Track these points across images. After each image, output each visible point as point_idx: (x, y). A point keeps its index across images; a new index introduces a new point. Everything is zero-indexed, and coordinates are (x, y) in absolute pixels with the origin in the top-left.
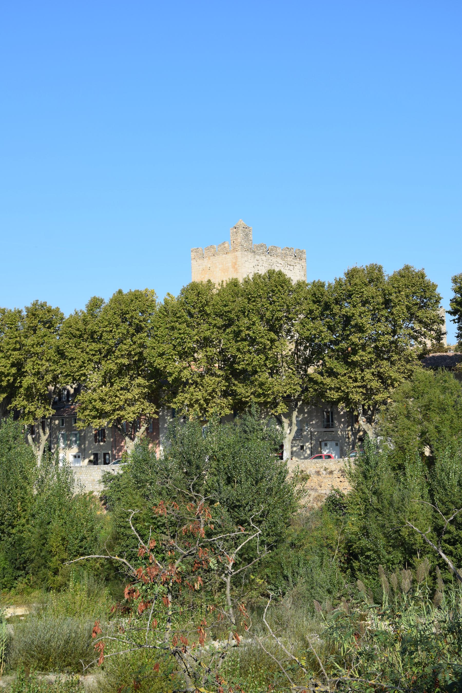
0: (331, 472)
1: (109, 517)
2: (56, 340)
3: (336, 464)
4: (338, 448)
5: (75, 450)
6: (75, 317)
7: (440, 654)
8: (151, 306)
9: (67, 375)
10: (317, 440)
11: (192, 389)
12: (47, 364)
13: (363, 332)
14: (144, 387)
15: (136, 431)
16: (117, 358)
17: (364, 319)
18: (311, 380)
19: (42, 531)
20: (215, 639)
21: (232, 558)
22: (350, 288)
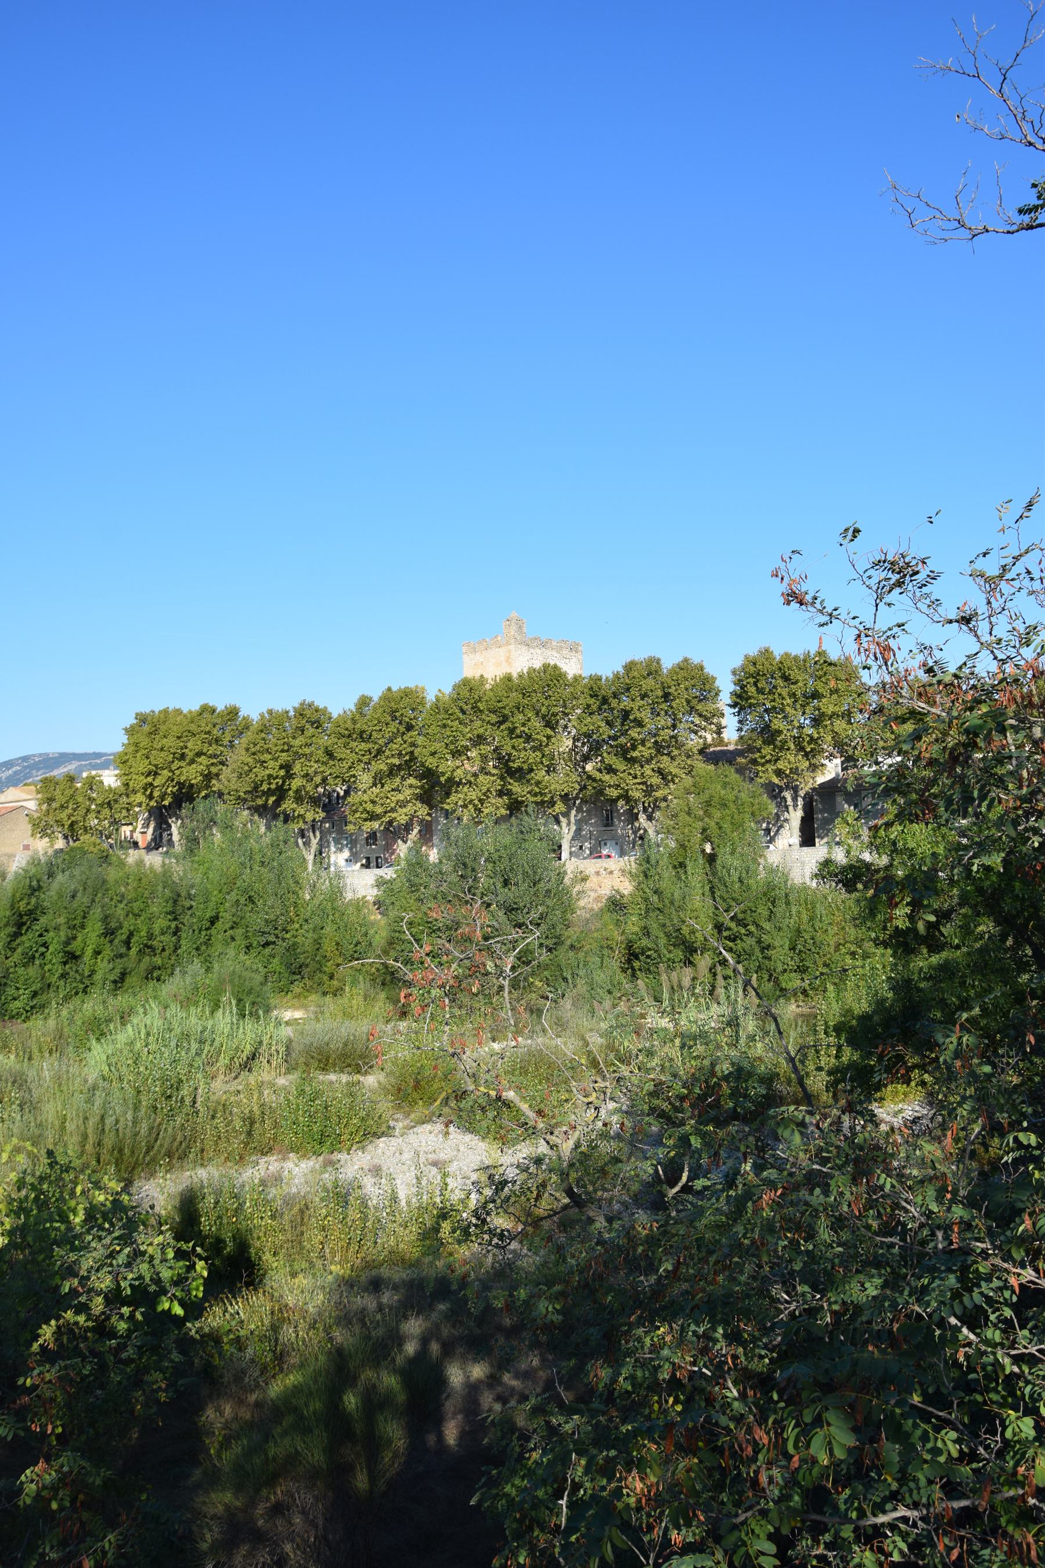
0: (611, 873)
1: (383, 922)
2: (325, 740)
3: (616, 863)
4: (618, 847)
5: (346, 854)
6: (343, 717)
7: (719, 1047)
8: (422, 703)
9: (337, 777)
10: (596, 839)
11: (465, 789)
12: (316, 765)
13: (642, 726)
14: (416, 787)
15: (408, 834)
16: (387, 757)
17: (644, 713)
18: (589, 777)
19: (316, 937)
20: (494, 1041)
21: (510, 961)
22: (628, 681)
